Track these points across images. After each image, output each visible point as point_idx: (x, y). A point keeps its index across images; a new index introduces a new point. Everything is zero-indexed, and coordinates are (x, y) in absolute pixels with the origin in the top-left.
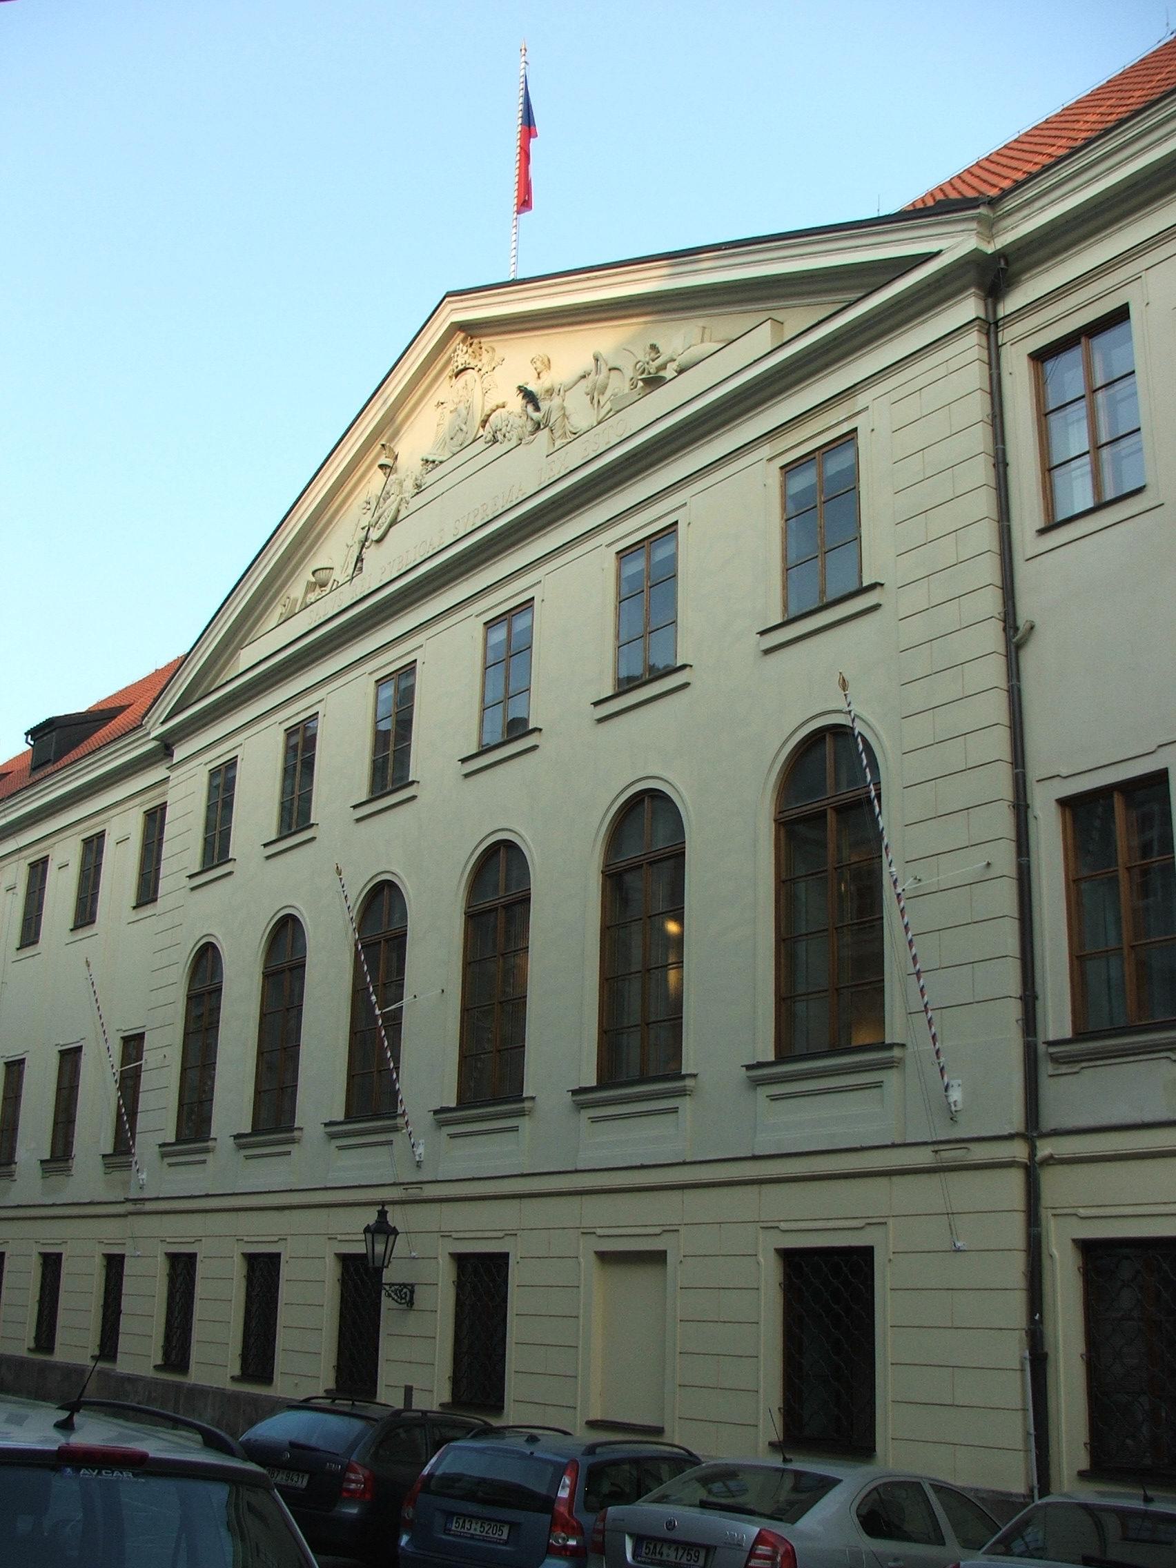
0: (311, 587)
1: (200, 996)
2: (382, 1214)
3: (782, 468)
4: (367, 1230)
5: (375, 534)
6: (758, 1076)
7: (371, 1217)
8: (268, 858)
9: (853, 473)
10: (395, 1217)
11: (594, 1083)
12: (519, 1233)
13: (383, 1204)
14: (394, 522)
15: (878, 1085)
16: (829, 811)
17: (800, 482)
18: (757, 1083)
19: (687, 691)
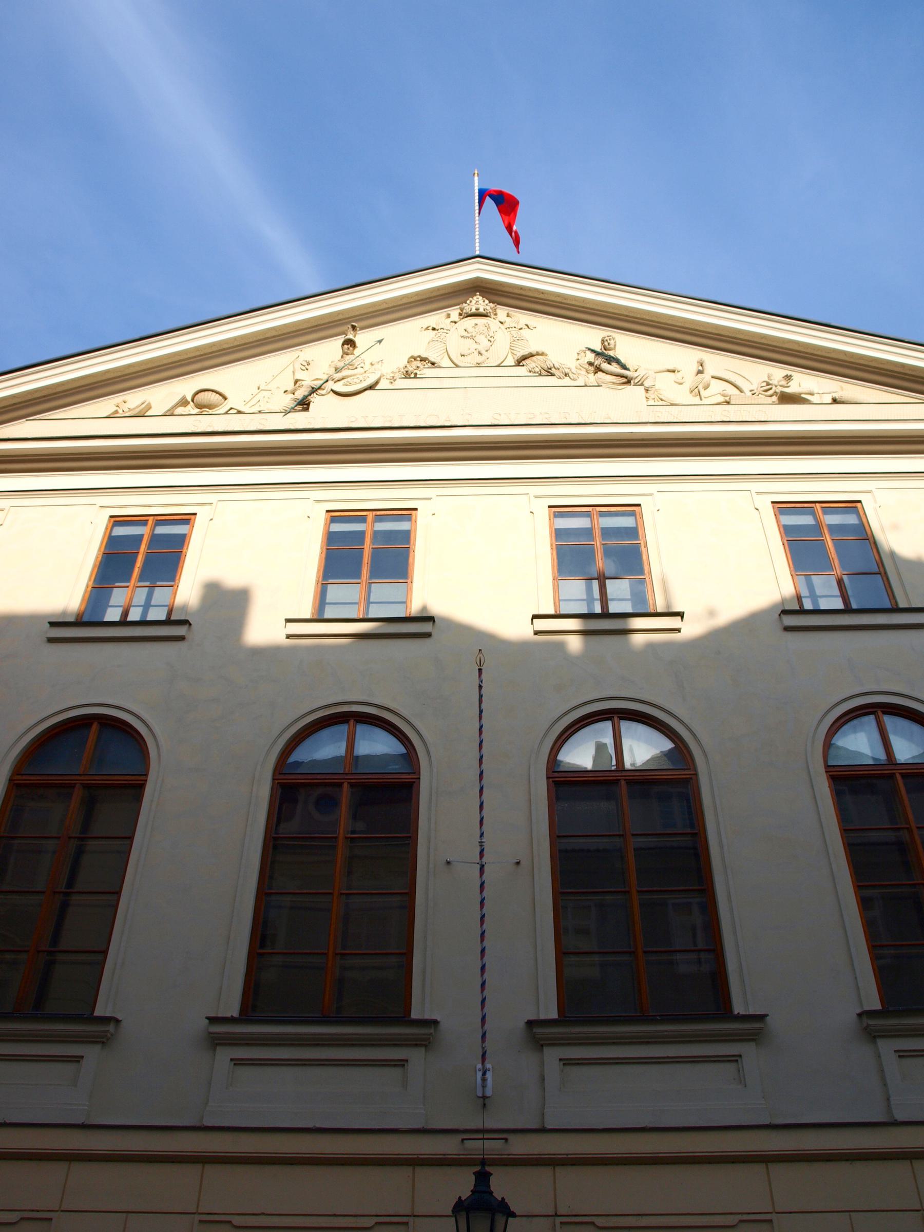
1: (19, 786)
2: (483, 1178)
3: (111, 517)
4: (460, 1207)
6: (218, 1035)
7: (463, 1184)
8: (51, 640)
10: (502, 1185)
11: (235, 1013)
12: (411, 1219)
13: (483, 1162)
14: (371, 387)
15: (77, 1059)
16: (346, 785)
18: (215, 1042)
19: (427, 641)
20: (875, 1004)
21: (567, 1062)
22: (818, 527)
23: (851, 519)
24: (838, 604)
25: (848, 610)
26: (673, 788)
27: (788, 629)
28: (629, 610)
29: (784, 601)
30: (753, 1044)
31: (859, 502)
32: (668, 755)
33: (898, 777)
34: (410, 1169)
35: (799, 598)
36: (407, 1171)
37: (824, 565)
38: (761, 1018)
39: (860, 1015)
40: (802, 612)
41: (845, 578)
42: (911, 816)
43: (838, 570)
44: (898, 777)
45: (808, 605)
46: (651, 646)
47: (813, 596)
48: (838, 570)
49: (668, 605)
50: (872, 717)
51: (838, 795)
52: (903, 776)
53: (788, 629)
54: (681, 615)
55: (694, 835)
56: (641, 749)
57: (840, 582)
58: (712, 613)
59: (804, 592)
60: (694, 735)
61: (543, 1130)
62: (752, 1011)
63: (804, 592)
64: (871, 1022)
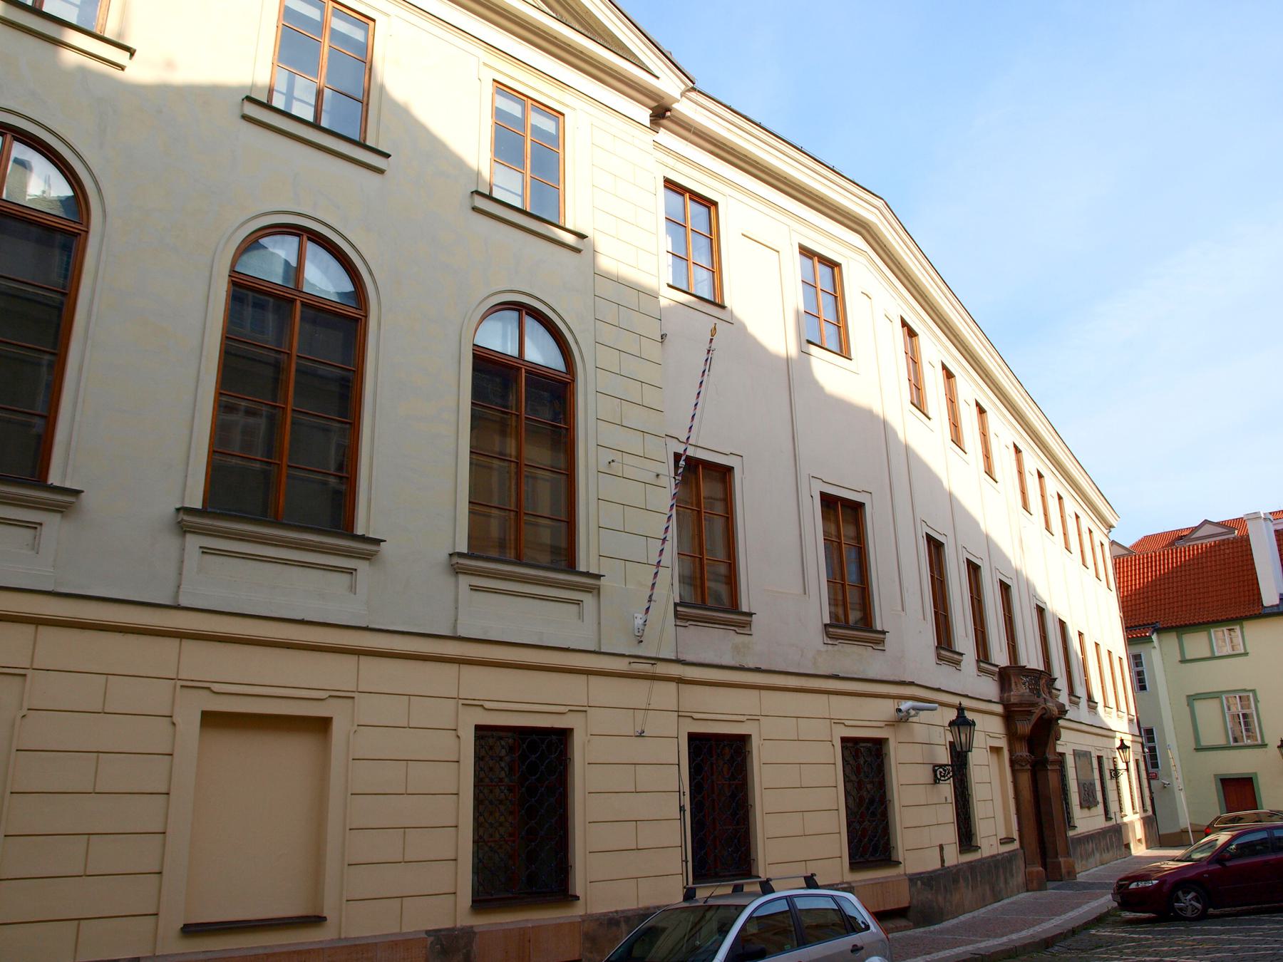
4: (952, 724)
7: (952, 715)
20: (464, 549)
21: (206, 551)
22: (321, 26)
23: (358, 35)
24: (310, 117)
25: (315, 125)
26: (346, 322)
27: (246, 118)
28: (74, 21)
29: (253, 87)
30: (58, 516)
31: (374, 20)
32: (64, 202)
33: (298, 303)
34: (178, 640)
35: (271, 91)
36: (30, 629)
37: (310, 68)
38: (77, 493)
39: (178, 510)
40: (268, 106)
41: (327, 93)
42: (295, 344)
43: (323, 81)
44: (298, 303)
45: (278, 102)
46: (82, 70)
47: (290, 96)
48: (323, 81)
49: (120, 35)
50: (296, 239)
51: (475, 369)
52: (303, 304)
53: (246, 118)
54: (131, 52)
55: (64, 294)
56: (322, 278)
57: (319, 94)
58: (170, 65)
59: (281, 86)
60: (99, 190)
61: (178, 607)
62: (68, 485)
63: (281, 86)
64: (186, 518)
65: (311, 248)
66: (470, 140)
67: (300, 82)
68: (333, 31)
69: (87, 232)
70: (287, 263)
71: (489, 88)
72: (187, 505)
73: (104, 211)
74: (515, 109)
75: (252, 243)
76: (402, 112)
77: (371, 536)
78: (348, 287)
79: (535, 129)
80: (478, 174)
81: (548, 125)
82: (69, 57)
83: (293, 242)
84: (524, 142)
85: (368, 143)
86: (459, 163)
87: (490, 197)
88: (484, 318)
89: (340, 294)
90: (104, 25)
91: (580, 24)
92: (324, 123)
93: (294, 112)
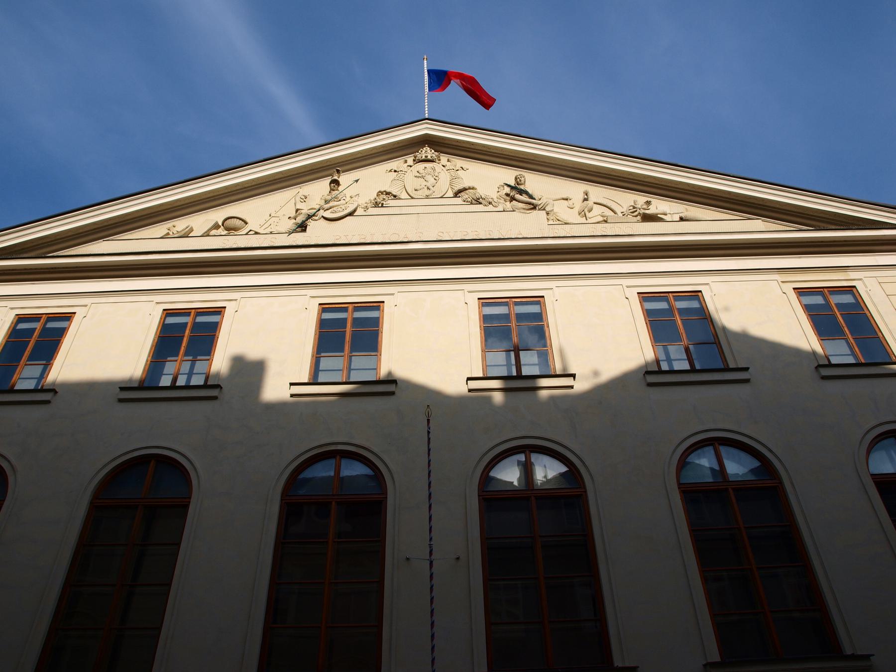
0: (216, 226)
5: (328, 214)
9: (62, 332)
17: (327, 316)
22: (670, 311)
23: (695, 304)
24: (686, 366)
25: (693, 370)
29: (647, 364)
35: (658, 362)
39: (705, 666)
40: (660, 372)
41: (691, 347)
45: (665, 367)
46: (552, 398)
47: (669, 360)
48: (686, 341)
49: (565, 368)
50: (711, 448)
53: (650, 385)
56: (737, 467)
57: (687, 350)
59: (662, 357)
65: (723, 450)
66: (795, 332)
67: (672, 349)
68: (679, 310)
69: (586, 492)
70: (712, 469)
71: (793, 296)
72: (709, 661)
73: (591, 475)
74: (818, 300)
75: (683, 464)
76: (744, 338)
77: (859, 653)
78: (756, 464)
79: (837, 305)
80: (814, 353)
81: (847, 299)
82: (544, 393)
83: (710, 450)
84: (835, 318)
85: (731, 366)
86: (796, 353)
87: (830, 365)
88: (869, 452)
89: (752, 471)
90: (555, 368)
91: (835, 224)
92: (698, 367)
93: (676, 368)
